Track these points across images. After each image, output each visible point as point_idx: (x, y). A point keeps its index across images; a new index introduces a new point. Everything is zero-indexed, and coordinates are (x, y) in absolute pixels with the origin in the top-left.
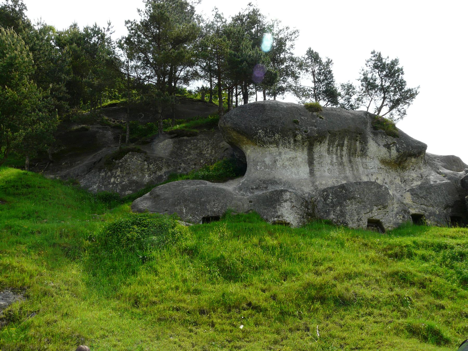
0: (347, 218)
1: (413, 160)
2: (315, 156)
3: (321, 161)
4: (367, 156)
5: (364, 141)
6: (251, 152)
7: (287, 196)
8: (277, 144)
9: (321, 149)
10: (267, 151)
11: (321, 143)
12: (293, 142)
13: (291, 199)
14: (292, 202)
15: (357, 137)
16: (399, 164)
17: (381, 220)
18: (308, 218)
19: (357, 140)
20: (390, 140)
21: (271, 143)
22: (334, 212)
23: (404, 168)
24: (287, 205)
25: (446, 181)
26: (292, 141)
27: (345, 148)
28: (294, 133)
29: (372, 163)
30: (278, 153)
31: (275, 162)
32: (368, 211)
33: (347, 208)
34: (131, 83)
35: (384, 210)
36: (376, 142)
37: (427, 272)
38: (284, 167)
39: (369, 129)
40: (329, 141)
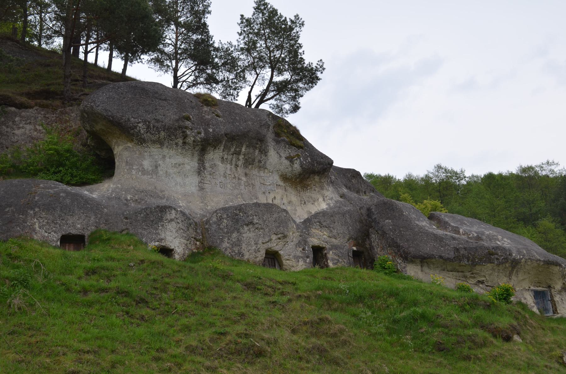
0: (243, 248)
1: (317, 178)
2: (207, 165)
3: (213, 171)
4: (266, 168)
5: (264, 152)
6: (122, 151)
9: (214, 156)
10: (146, 152)
13: (177, 219)
14: (178, 222)
15: (257, 144)
16: (301, 182)
17: (280, 252)
18: (196, 244)
19: (256, 148)
20: (293, 152)
21: (154, 142)
22: (229, 239)
23: (305, 187)
24: (172, 227)
27: (241, 157)
28: (184, 132)
29: (271, 178)
30: (161, 157)
35: (284, 240)
36: (277, 153)
37: (13, 93)
39: (270, 136)
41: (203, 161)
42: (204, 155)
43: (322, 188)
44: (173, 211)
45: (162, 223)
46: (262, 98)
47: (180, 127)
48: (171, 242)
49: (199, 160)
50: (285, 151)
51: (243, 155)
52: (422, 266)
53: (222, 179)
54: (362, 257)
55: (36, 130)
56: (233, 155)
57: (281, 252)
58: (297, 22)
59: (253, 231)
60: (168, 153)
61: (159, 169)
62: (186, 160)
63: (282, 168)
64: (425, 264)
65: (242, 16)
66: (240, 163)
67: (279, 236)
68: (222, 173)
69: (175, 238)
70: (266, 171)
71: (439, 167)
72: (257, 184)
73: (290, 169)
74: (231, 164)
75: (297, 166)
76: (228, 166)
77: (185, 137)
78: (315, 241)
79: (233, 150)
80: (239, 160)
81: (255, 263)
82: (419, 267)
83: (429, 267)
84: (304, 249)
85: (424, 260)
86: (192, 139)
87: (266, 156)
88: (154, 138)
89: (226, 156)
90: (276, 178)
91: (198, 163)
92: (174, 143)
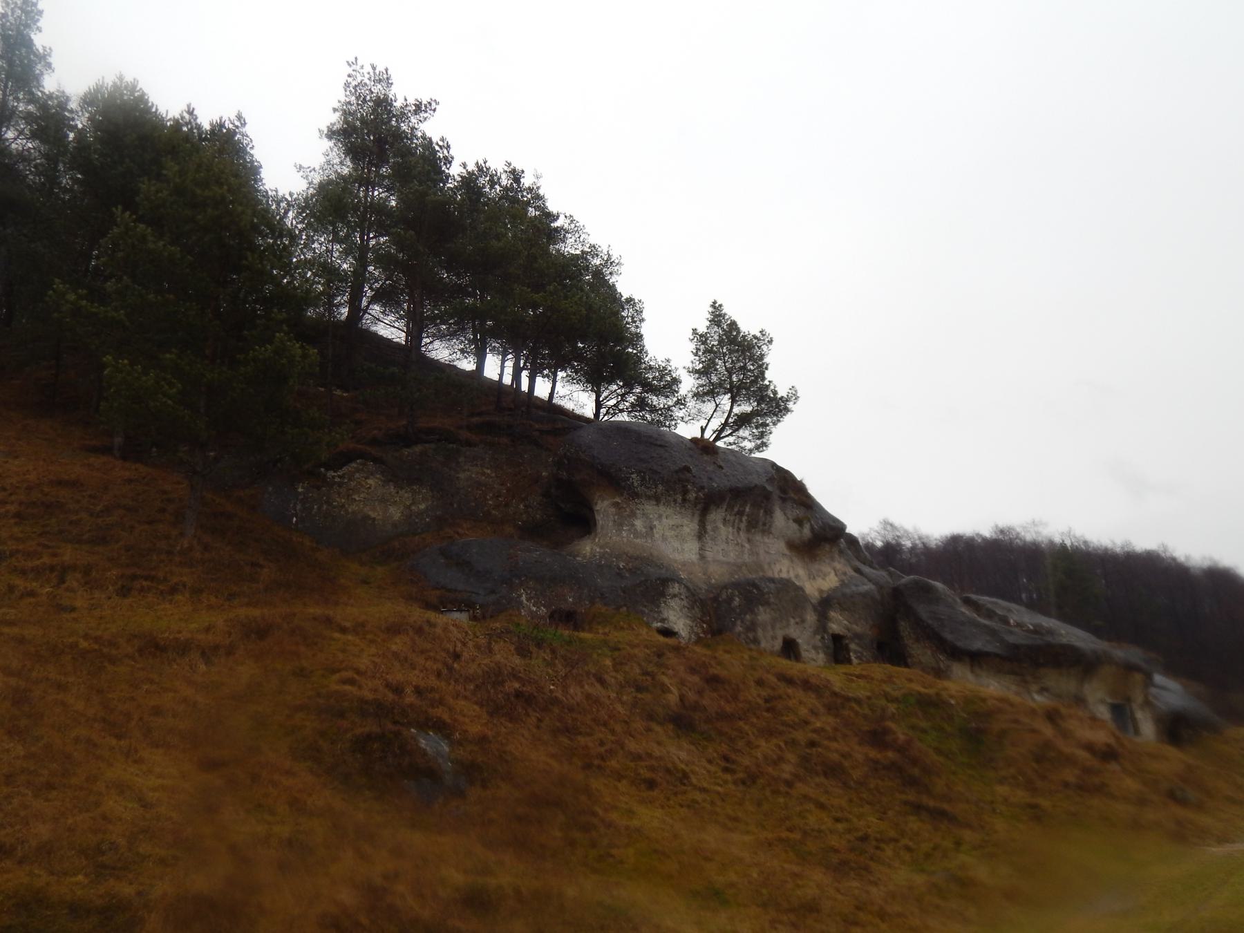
1: (827, 547)
2: (709, 528)
5: (769, 512)
6: (604, 507)
7: (675, 588)
8: (657, 499)
9: (716, 516)
20: (799, 512)
21: (649, 498)
24: (674, 603)
25: (868, 587)
27: (744, 518)
28: (685, 487)
31: (651, 528)
38: (664, 538)
43: (833, 559)
44: (677, 585)
46: (719, 435)
53: (724, 546)
54: (889, 649)
55: (484, 474)
57: (799, 641)
58: (763, 339)
62: (685, 522)
65: (695, 330)
66: (743, 526)
72: (761, 552)
74: (733, 526)
75: (807, 531)
76: (730, 529)
77: (685, 492)
78: (834, 627)
81: (772, 653)
84: (823, 638)
85: (976, 659)
88: (649, 493)
90: (781, 546)
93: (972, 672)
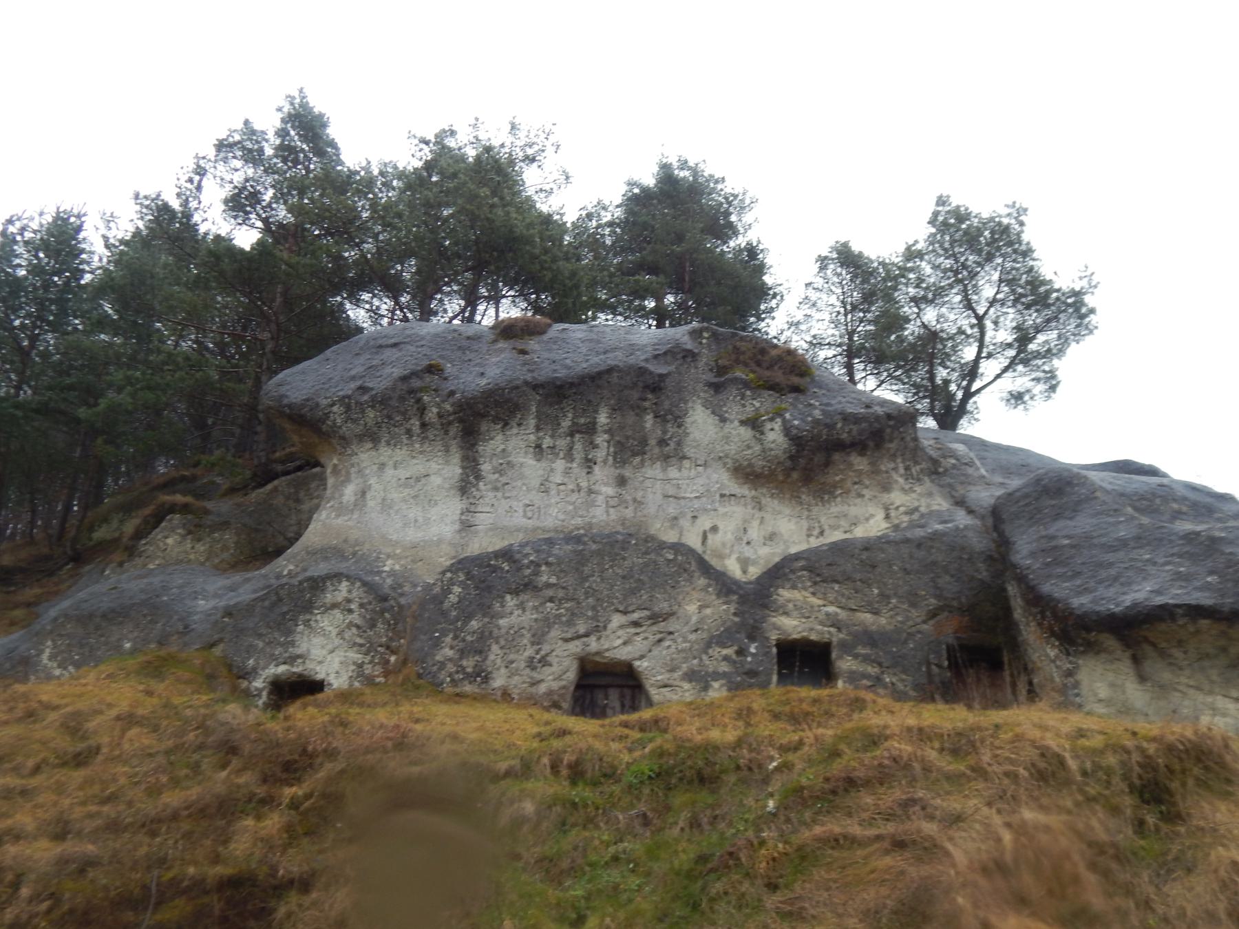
1: (860, 463)
2: (486, 467)
3: (504, 480)
4: (684, 457)
5: (673, 417)
9: (510, 446)
11: (506, 424)
12: (419, 431)
16: (807, 479)
17: (637, 663)
21: (361, 438)
22: (455, 637)
23: (825, 493)
24: (329, 623)
26: (416, 429)
27: (601, 439)
28: (419, 400)
29: (700, 481)
30: (375, 468)
32: (582, 631)
33: (502, 622)
34: (49, 323)
35: (655, 628)
38: (386, 505)
40: (537, 417)
41: (475, 460)
42: (474, 445)
43: (886, 488)
45: (308, 617)
47: (412, 391)
48: (320, 662)
49: (465, 458)
50: (744, 406)
51: (606, 432)
52: (1136, 660)
56: (572, 435)
57: (641, 665)
59: (535, 608)
60: (391, 457)
61: (368, 496)
62: (434, 466)
63: (732, 448)
64: (1147, 648)
67: (636, 616)
68: (535, 482)
69: (332, 652)
70: (686, 463)
71: (631, 184)
73: (757, 448)
74: (569, 457)
75: (775, 436)
76: (560, 465)
79: (566, 424)
80: (596, 447)
82: (1126, 666)
83: (1174, 665)
86: (435, 410)
87: (679, 426)
89: (547, 442)
90: (721, 478)
91: (463, 468)
92: (403, 431)
93: (1142, 678)
